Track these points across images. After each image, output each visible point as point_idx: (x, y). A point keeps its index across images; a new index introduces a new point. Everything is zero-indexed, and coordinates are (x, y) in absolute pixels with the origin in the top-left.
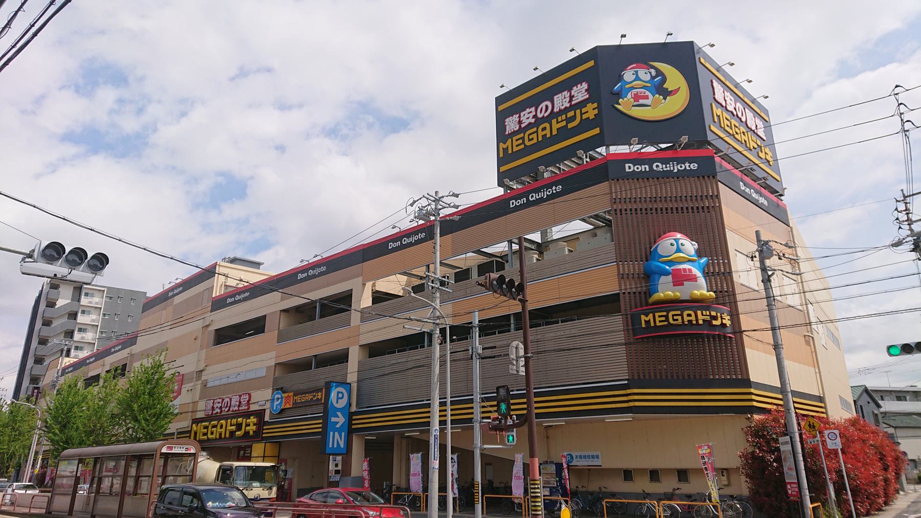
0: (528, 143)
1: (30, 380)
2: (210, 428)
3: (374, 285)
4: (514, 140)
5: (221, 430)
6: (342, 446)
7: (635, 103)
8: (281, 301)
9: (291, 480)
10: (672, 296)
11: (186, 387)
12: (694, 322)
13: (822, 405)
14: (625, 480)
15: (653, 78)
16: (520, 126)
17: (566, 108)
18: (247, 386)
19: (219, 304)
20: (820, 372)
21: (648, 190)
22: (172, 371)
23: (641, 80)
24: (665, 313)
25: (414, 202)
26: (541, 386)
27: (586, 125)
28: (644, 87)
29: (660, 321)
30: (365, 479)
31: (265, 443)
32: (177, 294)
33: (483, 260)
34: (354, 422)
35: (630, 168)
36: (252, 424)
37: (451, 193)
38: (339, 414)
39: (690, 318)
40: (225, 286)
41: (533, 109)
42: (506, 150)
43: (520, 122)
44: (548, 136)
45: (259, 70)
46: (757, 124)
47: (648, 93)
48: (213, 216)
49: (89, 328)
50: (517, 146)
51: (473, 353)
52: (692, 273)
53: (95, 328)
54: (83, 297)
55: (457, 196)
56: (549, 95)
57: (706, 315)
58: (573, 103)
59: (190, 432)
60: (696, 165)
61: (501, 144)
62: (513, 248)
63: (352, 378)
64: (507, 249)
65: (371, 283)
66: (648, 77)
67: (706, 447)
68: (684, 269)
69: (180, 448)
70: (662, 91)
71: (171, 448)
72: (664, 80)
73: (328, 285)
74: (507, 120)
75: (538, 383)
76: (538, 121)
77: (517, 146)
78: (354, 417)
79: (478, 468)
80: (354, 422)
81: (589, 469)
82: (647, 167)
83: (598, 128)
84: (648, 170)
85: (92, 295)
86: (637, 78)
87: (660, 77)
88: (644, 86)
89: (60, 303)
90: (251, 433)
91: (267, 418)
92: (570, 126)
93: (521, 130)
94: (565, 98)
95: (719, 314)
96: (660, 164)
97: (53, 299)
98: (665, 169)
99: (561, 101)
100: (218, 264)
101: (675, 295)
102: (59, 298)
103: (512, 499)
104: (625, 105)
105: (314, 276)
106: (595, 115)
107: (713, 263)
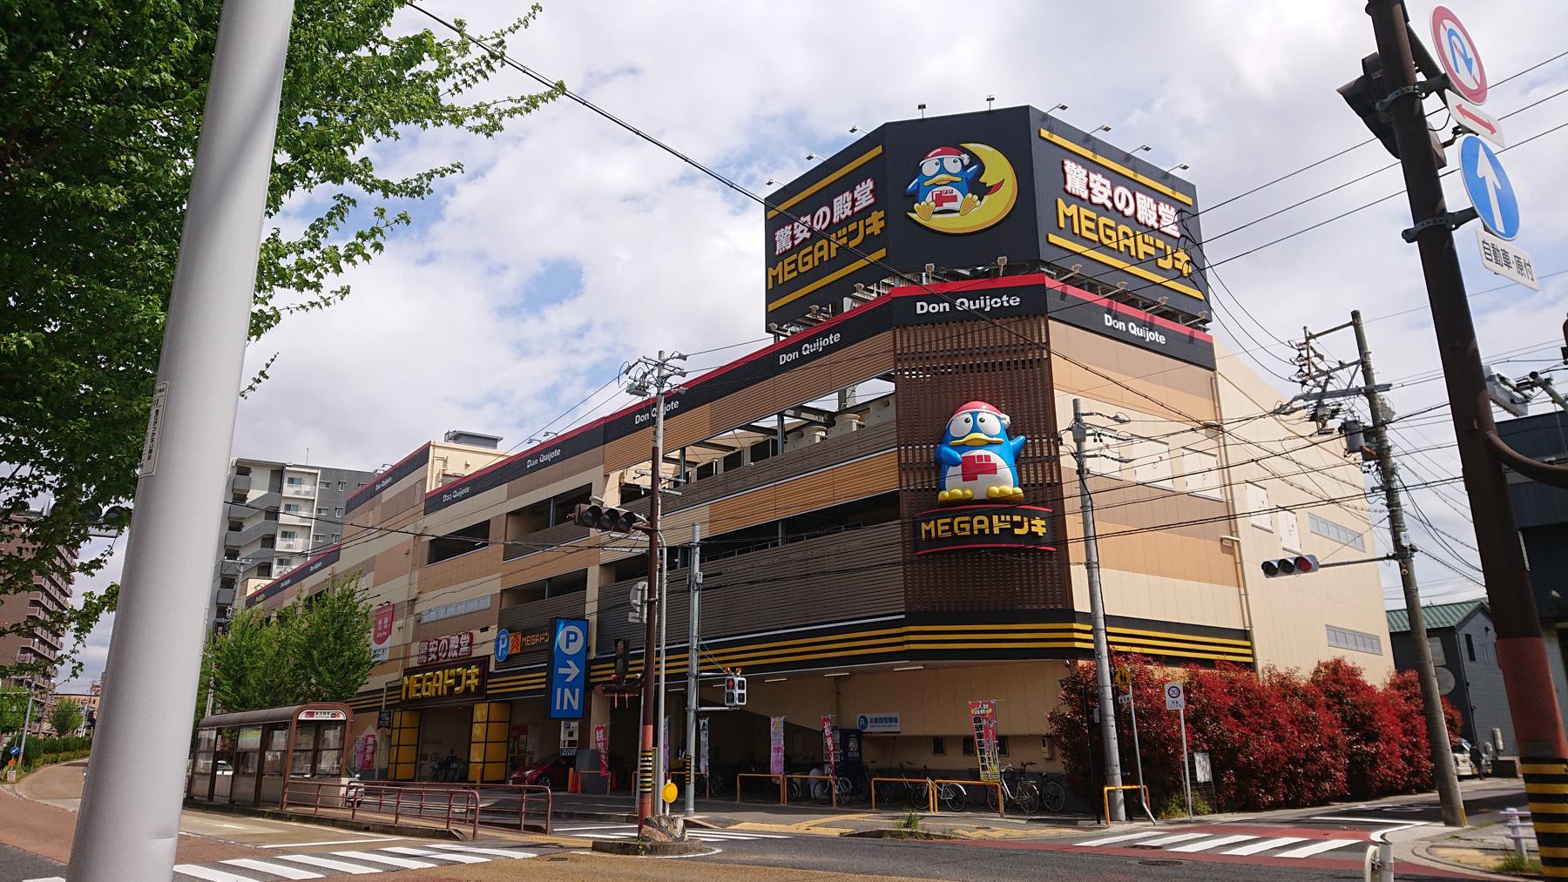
0: (802, 269)
1: (218, 611)
2: (424, 681)
3: (622, 476)
4: (786, 265)
5: (437, 685)
6: (576, 708)
7: (938, 209)
8: (508, 499)
9: (531, 754)
10: (959, 495)
11: (398, 623)
12: (987, 531)
13: (1247, 643)
14: (964, 753)
15: (965, 168)
16: (793, 243)
17: (847, 216)
18: (466, 623)
19: (435, 502)
20: (1246, 594)
21: (945, 339)
22: (382, 600)
23: (948, 173)
24: (949, 520)
25: (630, 368)
26: (809, 622)
27: (870, 243)
28: (951, 183)
29: (943, 531)
30: (601, 754)
31: (489, 703)
32: (386, 488)
33: (759, 438)
34: (593, 674)
35: (922, 308)
36: (473, 677)
37: (676, 355)
38: (570, 663)
39: (981, 526)
40: (444, 475)
41: (808, 218)
42: (775, 278)
43: (793, 237)
44: (826, 259)
45: (616, 74)
46: (1160, 213)
47: (956, 192)
48: (532, 328)
49: (298, 531)
50: (789, 272)
51: (690, 583)
52: (990, 461)
53: (307, 530)
54: (285, 485)
55: (684, 358)
56: (827, 197)
57: (1005, 521)
58: (856, 209)
59: (400, 687)
60: (1018, 300)
61: (770, 269)
62: (786, 422)
63: (591, 608)
64: (776, 424)
65: (619, 473)
66: (957, 168)
67: (987, 706)
68: (980, 457)
69: (325, 713)
70: (977, 187)
71: (312, 714)
72: (982, 169)
73: (539, 486)
74: (778, 233)
75: (806, 619)
76: (815, 236)
77: (789, 272)
78: (593, 667)
79: (691, 734)
80: (593, 674)
81: (894, 738)
82: (947, 305)
83: (884, 250)
84: (947, 309)
85: (300, 482)
86: (943, 170)
87: (975, 167)
88: (952, 181)
89: (253, 495)
90: (473, 689)
91: (492, 669)
92: (852, 244)
93: (795, 249)
94: (846, 202)
95: (1026, 519)
96: (965, 300)
97: (242, 491)
98: (972, 307)
99: (842, 207)
100: (432, 444)
101: (964, 494)
102: (249, 485)
103: (773, 780)
104: (924, 213)
105: (547, 464)
106: (881, 229)
107: (1033, 443)
